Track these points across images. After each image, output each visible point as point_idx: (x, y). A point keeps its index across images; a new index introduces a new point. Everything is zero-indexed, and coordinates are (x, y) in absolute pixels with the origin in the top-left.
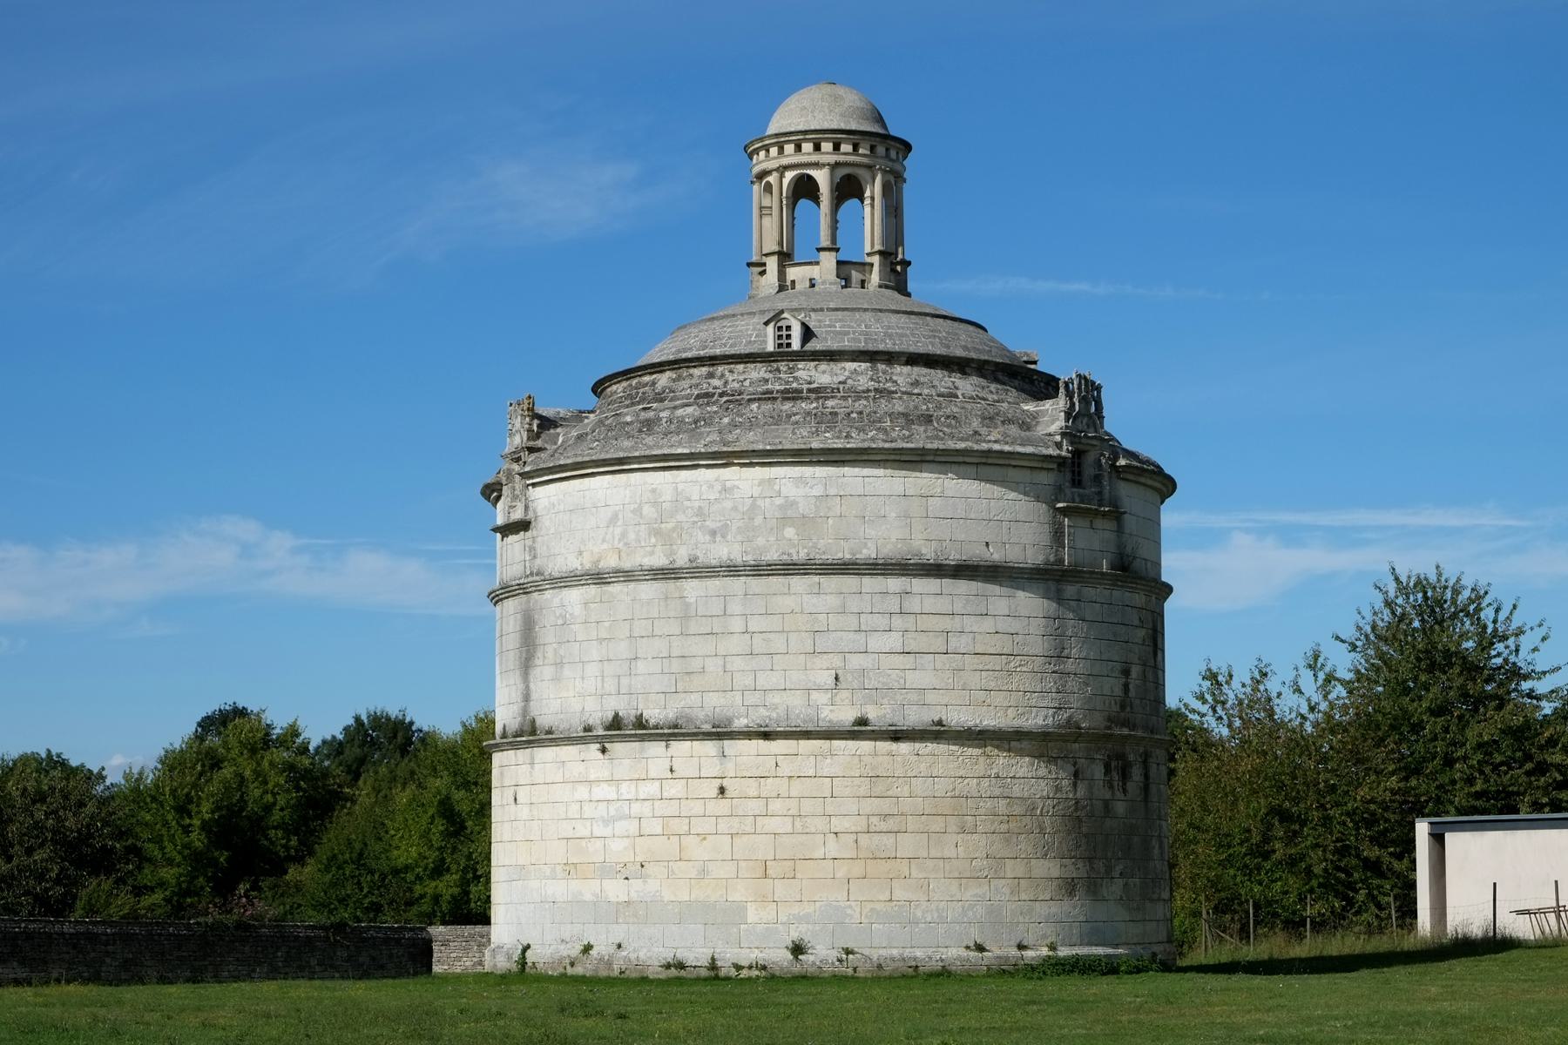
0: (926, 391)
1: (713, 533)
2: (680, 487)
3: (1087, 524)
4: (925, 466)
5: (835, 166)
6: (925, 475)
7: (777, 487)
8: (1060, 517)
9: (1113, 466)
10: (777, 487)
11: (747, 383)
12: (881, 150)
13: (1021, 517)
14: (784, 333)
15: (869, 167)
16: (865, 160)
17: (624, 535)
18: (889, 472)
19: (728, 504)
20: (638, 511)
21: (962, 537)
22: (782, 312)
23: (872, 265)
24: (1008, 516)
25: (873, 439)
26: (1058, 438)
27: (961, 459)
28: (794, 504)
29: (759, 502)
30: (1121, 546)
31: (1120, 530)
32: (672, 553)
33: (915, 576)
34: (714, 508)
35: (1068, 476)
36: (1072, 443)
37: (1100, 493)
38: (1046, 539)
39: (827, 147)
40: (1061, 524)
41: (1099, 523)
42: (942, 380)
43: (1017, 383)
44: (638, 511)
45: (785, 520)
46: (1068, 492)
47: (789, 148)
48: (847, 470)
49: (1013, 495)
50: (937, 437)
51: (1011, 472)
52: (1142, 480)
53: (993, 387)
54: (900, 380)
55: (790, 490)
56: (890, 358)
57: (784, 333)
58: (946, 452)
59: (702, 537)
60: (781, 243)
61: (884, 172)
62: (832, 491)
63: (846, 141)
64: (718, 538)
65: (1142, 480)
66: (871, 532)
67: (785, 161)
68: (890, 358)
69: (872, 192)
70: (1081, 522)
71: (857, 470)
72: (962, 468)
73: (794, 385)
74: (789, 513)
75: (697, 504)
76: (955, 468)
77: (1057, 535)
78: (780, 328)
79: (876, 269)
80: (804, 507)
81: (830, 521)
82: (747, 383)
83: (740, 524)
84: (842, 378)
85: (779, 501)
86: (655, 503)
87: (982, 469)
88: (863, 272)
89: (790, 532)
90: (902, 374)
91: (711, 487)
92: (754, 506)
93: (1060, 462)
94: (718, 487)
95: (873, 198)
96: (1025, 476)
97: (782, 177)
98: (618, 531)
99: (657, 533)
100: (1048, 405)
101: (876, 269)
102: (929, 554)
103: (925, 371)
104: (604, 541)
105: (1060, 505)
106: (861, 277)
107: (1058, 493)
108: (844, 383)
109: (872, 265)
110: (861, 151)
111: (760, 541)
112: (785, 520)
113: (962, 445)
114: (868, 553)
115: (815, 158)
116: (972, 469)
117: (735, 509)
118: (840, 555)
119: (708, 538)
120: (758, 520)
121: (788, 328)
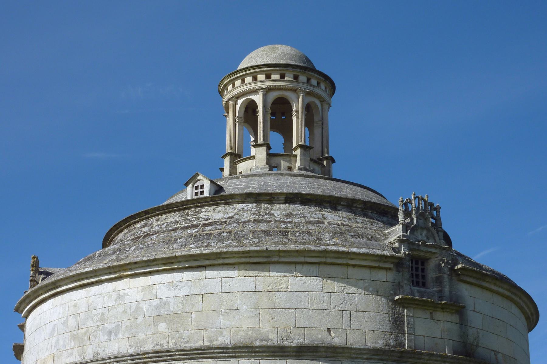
0: (296, 220)
1: (110, 333)
2: (91, 299)
3: (428, 315)
4: (272, 266)
5: (268, 90)
6: (272, 274)
7: (154, 292)
8: (399, 309)
9: (452, 269)
10: (154, 292)
11: (164, 226)
12: (303, 78)
13: (360, 307)
14: (199, 190)
15: (295, 91)
16: (289, 84)
17: (57, 343)
18: (242, 272)
19: (120, 309)
20: (65, 323)
21: (306, 324)
22: (197, 175)
23: (296, 156)
24: (348, 307)
25: (226, 246)
26: (397, 245)
27: (302, 259)
28: (166, 304)
29: (142, 305)
30: (464, 335)
31: (463, 322)
32: (83, 353)
33: (263, 357)
34: (111, 313)
35: (407, 275)
36: (410, 250)
37: (441, 291)
38: (386, 327)
39: (261, 77)
40: (401, 315)
41: (439, 315)
42: (313, 212)
43: (385, 219)
44: (65, 323)
45: (159, 318)
46: (407, 288)
47: (249, 79)
48: (208, 273)
49: (352, 289)
50: (282, 243)
51: (351, 271)
52: (485, 284)
53: (359, 219)
54: (277, 214)
55: (164, 293)
56: (271, 198)
57: (199, 190)
58: (287, 253)
59: (103, 337)
60: (233, 148)
61: (308, 94)
62: (196, 291)
63: (275, 72)
64: (113, 337)
65: (485, 284)
66: (226, 322)
67: (236, 92)
68: (271, 198)
69: (297, 107)
70: (420, 313)
71: (216, 272)
72: (306, 268)
73: (195, 223)
74: (163, 311)
75: (100, 311)
76: (299, 267)
77: (397, 323)
78: (197, 188)
79: (298, 158)
80: (174, 306)
81: (193, 315)
82: (164, 226)
83: (128, 323)
84: (230, 215)
85: (155, 302)
86: (75, 315)
87: (323, 268)
88: (290, 162)
89: (162, 327)
90: (279, 210)
91: (110, 296)
92: (138, 309)
93: (398, 263)
94: (115, 296)
95: (297, 111)
96: (366, 274)
97: (236, 104)
98: (54, 340)
99: (75, 338)
100: (397, 226)
101: (298, 158)
102: (275, 339)
103: (299, 207)
104: (47, 349)
105: (397, 298)
106: (288, 164)
107: (397, 287)
108: (232, 217)
109: (296, 156)
110: (286, 78)
111: (141, 336)
112: (159, 318)
113: (301, 247)
114: (224, 340)
115: (253, 86)
116: (315, 269)
117: (125, 312)
118: (200, 343)
119: (106, 337)
120: (141, 319)
121: (202, 186)
